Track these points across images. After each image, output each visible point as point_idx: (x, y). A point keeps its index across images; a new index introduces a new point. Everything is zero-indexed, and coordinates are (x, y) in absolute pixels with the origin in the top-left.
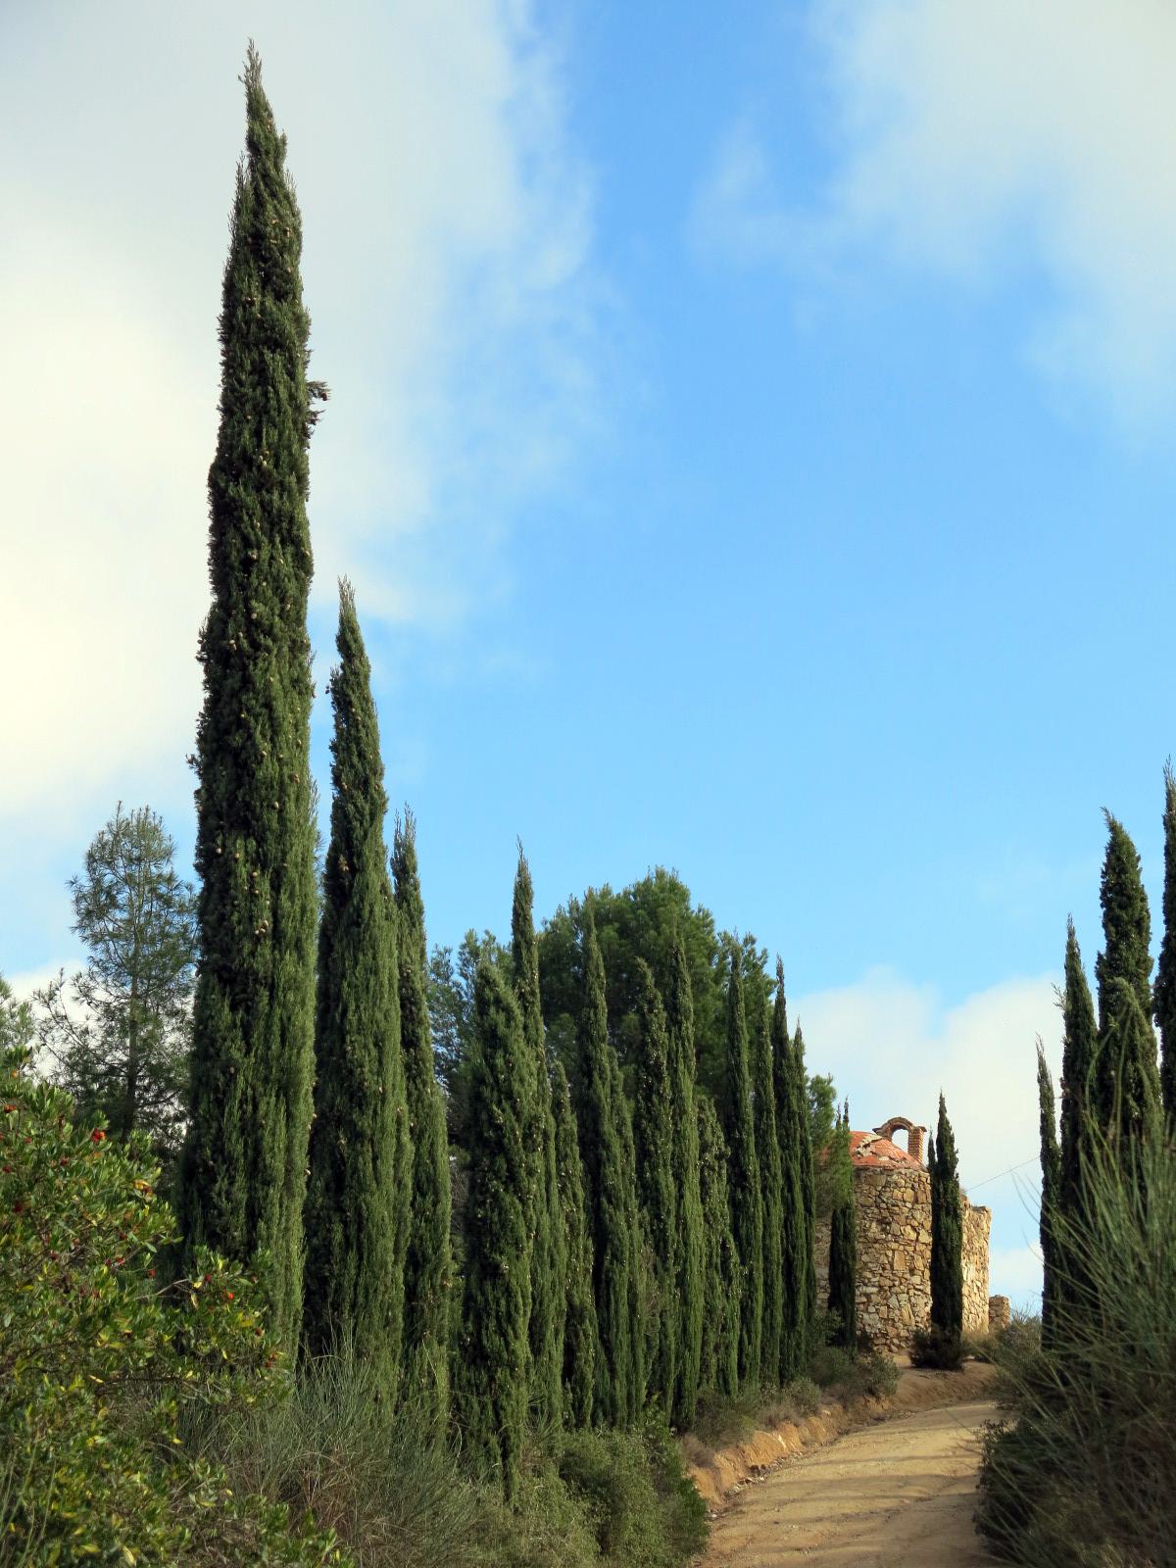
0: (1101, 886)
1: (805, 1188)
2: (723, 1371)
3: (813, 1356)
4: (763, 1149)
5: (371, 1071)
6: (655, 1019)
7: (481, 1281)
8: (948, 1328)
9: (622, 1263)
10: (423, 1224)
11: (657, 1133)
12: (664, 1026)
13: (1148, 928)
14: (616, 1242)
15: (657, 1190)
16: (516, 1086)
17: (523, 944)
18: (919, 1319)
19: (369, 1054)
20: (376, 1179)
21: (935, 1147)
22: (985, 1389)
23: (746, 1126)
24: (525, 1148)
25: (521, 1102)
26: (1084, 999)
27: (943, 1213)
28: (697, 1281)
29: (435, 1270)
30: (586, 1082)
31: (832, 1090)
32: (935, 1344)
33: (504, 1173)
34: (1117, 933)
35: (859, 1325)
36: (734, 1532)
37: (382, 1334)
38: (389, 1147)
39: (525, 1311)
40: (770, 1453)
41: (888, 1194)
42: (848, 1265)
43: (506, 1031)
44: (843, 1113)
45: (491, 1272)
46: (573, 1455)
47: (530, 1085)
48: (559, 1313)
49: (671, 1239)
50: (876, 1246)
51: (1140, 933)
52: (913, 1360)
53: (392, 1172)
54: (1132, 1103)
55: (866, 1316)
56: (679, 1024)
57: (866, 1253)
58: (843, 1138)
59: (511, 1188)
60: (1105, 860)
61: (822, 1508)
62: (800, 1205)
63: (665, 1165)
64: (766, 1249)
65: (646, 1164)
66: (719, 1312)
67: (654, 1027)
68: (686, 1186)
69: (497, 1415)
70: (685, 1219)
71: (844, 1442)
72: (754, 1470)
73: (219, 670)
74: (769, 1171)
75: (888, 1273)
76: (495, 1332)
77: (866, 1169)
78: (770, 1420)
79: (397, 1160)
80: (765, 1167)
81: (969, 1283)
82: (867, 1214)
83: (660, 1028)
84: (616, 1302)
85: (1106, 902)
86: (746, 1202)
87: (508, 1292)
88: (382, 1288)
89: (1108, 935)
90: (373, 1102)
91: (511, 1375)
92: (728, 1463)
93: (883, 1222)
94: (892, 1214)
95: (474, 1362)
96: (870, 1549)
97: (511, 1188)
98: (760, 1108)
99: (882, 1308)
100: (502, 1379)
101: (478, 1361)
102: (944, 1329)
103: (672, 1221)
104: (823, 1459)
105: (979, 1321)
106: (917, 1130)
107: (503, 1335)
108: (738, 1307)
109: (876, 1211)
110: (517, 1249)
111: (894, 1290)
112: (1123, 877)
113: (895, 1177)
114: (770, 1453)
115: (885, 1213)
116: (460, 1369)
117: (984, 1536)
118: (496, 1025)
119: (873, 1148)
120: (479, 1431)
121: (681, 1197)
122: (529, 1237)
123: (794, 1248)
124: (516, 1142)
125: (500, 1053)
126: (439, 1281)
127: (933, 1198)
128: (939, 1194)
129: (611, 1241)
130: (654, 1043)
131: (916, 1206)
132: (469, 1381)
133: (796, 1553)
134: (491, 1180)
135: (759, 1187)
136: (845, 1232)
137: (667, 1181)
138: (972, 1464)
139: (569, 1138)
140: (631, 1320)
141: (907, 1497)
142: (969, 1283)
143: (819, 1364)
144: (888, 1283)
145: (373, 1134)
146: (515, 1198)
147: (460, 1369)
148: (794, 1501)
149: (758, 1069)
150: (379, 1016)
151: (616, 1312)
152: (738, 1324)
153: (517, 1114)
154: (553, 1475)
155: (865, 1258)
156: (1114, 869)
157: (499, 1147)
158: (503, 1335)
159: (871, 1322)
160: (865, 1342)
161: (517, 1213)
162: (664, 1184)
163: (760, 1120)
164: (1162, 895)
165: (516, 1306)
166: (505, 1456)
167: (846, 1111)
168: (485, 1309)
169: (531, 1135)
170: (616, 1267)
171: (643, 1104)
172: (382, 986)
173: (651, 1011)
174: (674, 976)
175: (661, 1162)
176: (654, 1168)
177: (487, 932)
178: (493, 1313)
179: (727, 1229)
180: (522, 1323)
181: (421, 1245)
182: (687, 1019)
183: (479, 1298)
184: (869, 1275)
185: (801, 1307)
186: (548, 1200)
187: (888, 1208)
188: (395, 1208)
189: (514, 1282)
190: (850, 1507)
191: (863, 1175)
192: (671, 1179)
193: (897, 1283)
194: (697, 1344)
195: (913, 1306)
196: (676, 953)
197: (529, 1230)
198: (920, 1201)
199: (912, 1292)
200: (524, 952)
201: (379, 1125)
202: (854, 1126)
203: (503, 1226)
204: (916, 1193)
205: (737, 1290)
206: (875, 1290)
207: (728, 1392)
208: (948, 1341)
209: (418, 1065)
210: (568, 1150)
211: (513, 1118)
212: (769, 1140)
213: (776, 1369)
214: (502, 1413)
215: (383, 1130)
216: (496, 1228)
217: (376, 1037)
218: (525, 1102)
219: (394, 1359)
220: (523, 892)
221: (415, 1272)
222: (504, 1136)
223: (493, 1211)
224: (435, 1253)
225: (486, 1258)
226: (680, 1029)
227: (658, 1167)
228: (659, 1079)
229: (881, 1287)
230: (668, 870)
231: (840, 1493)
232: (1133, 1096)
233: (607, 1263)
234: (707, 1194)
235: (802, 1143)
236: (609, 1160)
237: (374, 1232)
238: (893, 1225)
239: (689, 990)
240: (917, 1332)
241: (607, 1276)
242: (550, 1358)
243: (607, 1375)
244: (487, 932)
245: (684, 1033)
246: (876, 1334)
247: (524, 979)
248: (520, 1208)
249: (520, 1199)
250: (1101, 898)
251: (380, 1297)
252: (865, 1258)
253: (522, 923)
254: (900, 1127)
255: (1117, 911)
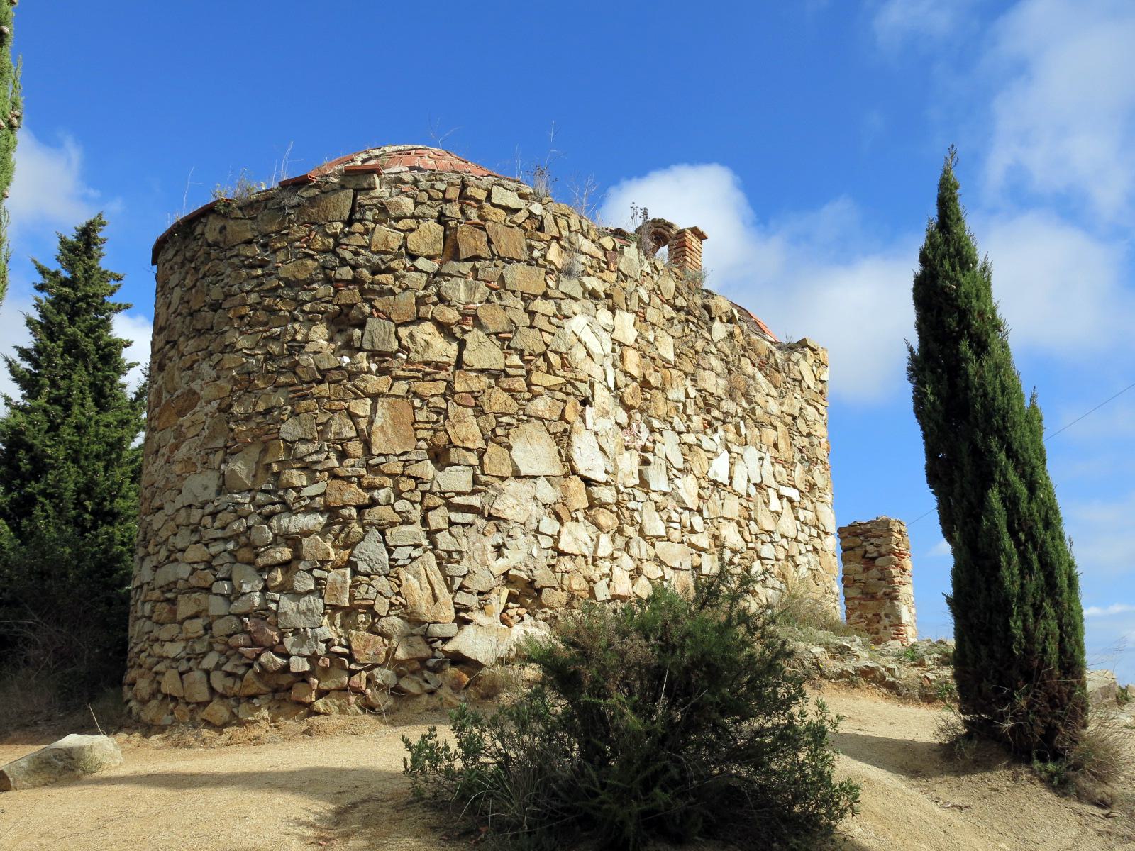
41: (357, 240)
55: (287, 604)
57: (295, 414)
73: (155, 729)
111: (372, 515)
115: (350, 295)
159: (301, 622)
184: (297, 477)
193: (381, 495)
198: (465, 252)
229: (332, 512)
238: (372, 324)
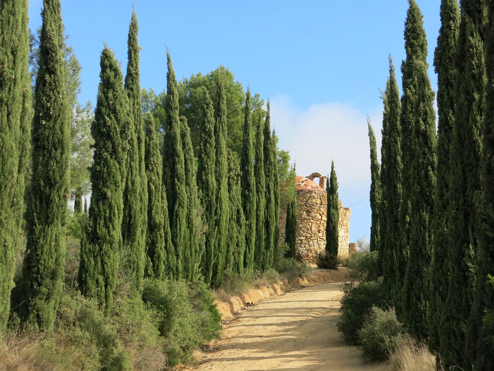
0: (404, 29)
1: (275, 194)
2: (237, 264)
3: (277, 261)
4: (257, 174)
5: (8, 67)
6: (209, 112)
7: (97, 201)
8: (332, 253)
9: (183, 208)
10: (55, 164)
11: (208, 160)
12: (213, 115)
13: (426, 49)
14: (181, 198)
15: (208, 184)
16: (118, 107)
17: (133, 51)
18: (321, 250)
19: (8, 58)
20: (9, 126)
21: (329, 182)
22: (346, 277)
23: (250, 164)
24: (121, 137)
25: (120, 115)
26: (395, 90)
27: (332, 208)
28: (224, 224)
29: (60, 187)
30: (169, 127)
31: (288, 156)
32: (327, 259)
33: (110, 150)
34: (412, 51)
35: (297, 251)
36: (234, 329)
37: (9, 210)
38: (17, 109)
39: (119, 217)
40: (256, 298)
41: (311, 201)
42: (293, 227)
43: (115, 80)
44: (293, 167)
45: (104, 197)
46: (150, 290)
47: (125, 107)
48: (144, 223)
49: (213, 205)
50: (305, 221)
51: (422, 51)
52: (318, 265)
53: (19, 122)
54: (421, 122)
55: (300, 248)
56: (220, 116)
58: (292, 176)
59: (114, 157)
60: (406, 17)
61: (274, 320)
62: (273, 200)
63: (211, 174)
64: (257, 216)
65: (203, 173)
66: (235, 238)
67: (209, 115)
68: (222, 184)
69: (103, 266)
70: (221, 198)
71: (288, 294)
72: (248, 304)
74: (260, 185)
75: (309, 232)
76: (104, 226)
77: (302, 191)
78: (257, 285)
79: (22, 118)
80: (258, 183)
81: (341, 237)
82: (302, 208)
83: (211, 116)
84: (180, 225)
85: (407, 37)
86: (249, 195)
87: (110, 207)
88: (9, 185)
89: (407, 52)
90: (9, 84)
91: (110, 247)
92: (237, 301)
93: (308, 212)
94: (312, 209)
95: (93, 240)
96: (292, 337)
97: (114, 157)
98: (257, 159)
99: (307, 245)
100: (106, 249)
101: (95, 240)
102: (331, 253)
103: (214, 197)
104: (277, 300)
105: (345, 252)
106: (323, 178)
107: (107, 227)
108: (244, 238)
109: (305, 207)
110: (116, 186)
111: (312, 238)
112: (415, 25)
113: (313, 194)
114: (256, 298)
115: (309, 208)
116: (85, 243)
117: (342, 333)
118: (109, 77)
119: (305, 183)
120: (94, 274)
121: (220, 189)
122: (122, 181)
123: (270, 217)
124: (117, 134)
125: (111, 91)
126: (62, 193)
127: (328, 201)
128: (330, 200)
129: (179, 198)
130: (209, 122)
131: (321, 206)
132: (90, 250)
133: (260, 338)
134: (103, 152)
135: (255, 189)
136: (292, 214)
137: (212, 179)
138: (338, 305)
139: (155, 147)
140: (190, 236)
141: (310, 316)
142: (341, 237)
143: (279, 264)
144: (309, 235)
145: (8, 101)
146: (115, 161)
147: (85, 243)
148: (262, 317)
149: (257, 147)
150: (14, 37)
151: (180, 229)
152: (244, 245)
153: (118, 121)
154: (138, 299)
155: (301, 226)
156: (411, 21)
157: (109, 136)
158: (107, 227)
159: (302, 251)
160: (299, 258)
161: (116, 169)
162: (211, 181)
163: (257, 164)
164: (439, 6)
165: (114, 214)
166: (106, 287)
167: (295, 166)
168: (98, 215)
169: (125, 131)
170: (181, 210)
171: (203, 147)
172: (17, 21)
173: (207, 108)
174: (219, 96)
175: (210, 172)
176: (206, 175)
177: (150, 89)
178: (103, 217)
179: (240, 205)
180: (118, 222)
181: (53, 174)
182: (224, 114)
183: (96, 209)
185: (272, 240)
186: (140, 170)
187: (310, 206)
188: (20, 143)
189: (113, 202)
190: (286, 320)
191: (301, 193)
192: (214, 179)
193: (313, 236)
194: (224, 250)
195: (319, 245)
196: (220, 87)
197: (123, 177)
198: (323, 204)
199: (319, 239)
200: (133, 55)
201: (12, 96)
202: (298, 173)
203: (109, 175)
204: (321, 201)
205: (244, 230)
206: (304, 238)
207: (239, 273)
208: (332, 258)
209: (55, 83)
210: (155, 152)
211: (116, 122)
212: (260, 172)
213: (261, 265)
214: (105, 265)
215: (14, 99)
216: (105, 175)
217: (12, 49)
218: (122, 115)
219: (18, 224)
220: (170, 77)
221: (50, 188)
222: (111, 131)
223: (104, 167)
224: (61, 179)
225: (100, 190)
226: (221, 119)
227: (208, 174)
228: (210, 137)
230: (226, 67)
231: (282, 314)
232: (422, 119)
233: (176, 208)
234: (231, 189)
235: (275, 176)
236: (179, 162)
237: (6, 154)
238: (312, 213)
239: (225, 102)
240: (320, 255)
241: (176, 213)
242: (139, 244)
243: (175, 257)
244: (150, 89)
245: (222, 120)
246: (304, 255)
247: (132, 67)
248: (118, 166)
249: (118, 162)
250: (404, 35)
251: (8, 190)
252: (301, 226)
253: (132, 41)
254: (316, 176)
255: (412, 41)
